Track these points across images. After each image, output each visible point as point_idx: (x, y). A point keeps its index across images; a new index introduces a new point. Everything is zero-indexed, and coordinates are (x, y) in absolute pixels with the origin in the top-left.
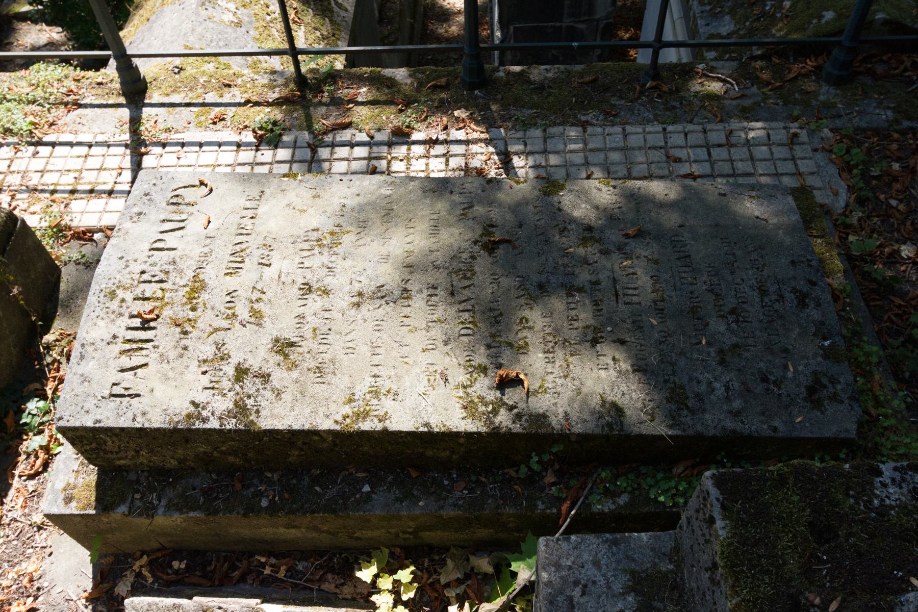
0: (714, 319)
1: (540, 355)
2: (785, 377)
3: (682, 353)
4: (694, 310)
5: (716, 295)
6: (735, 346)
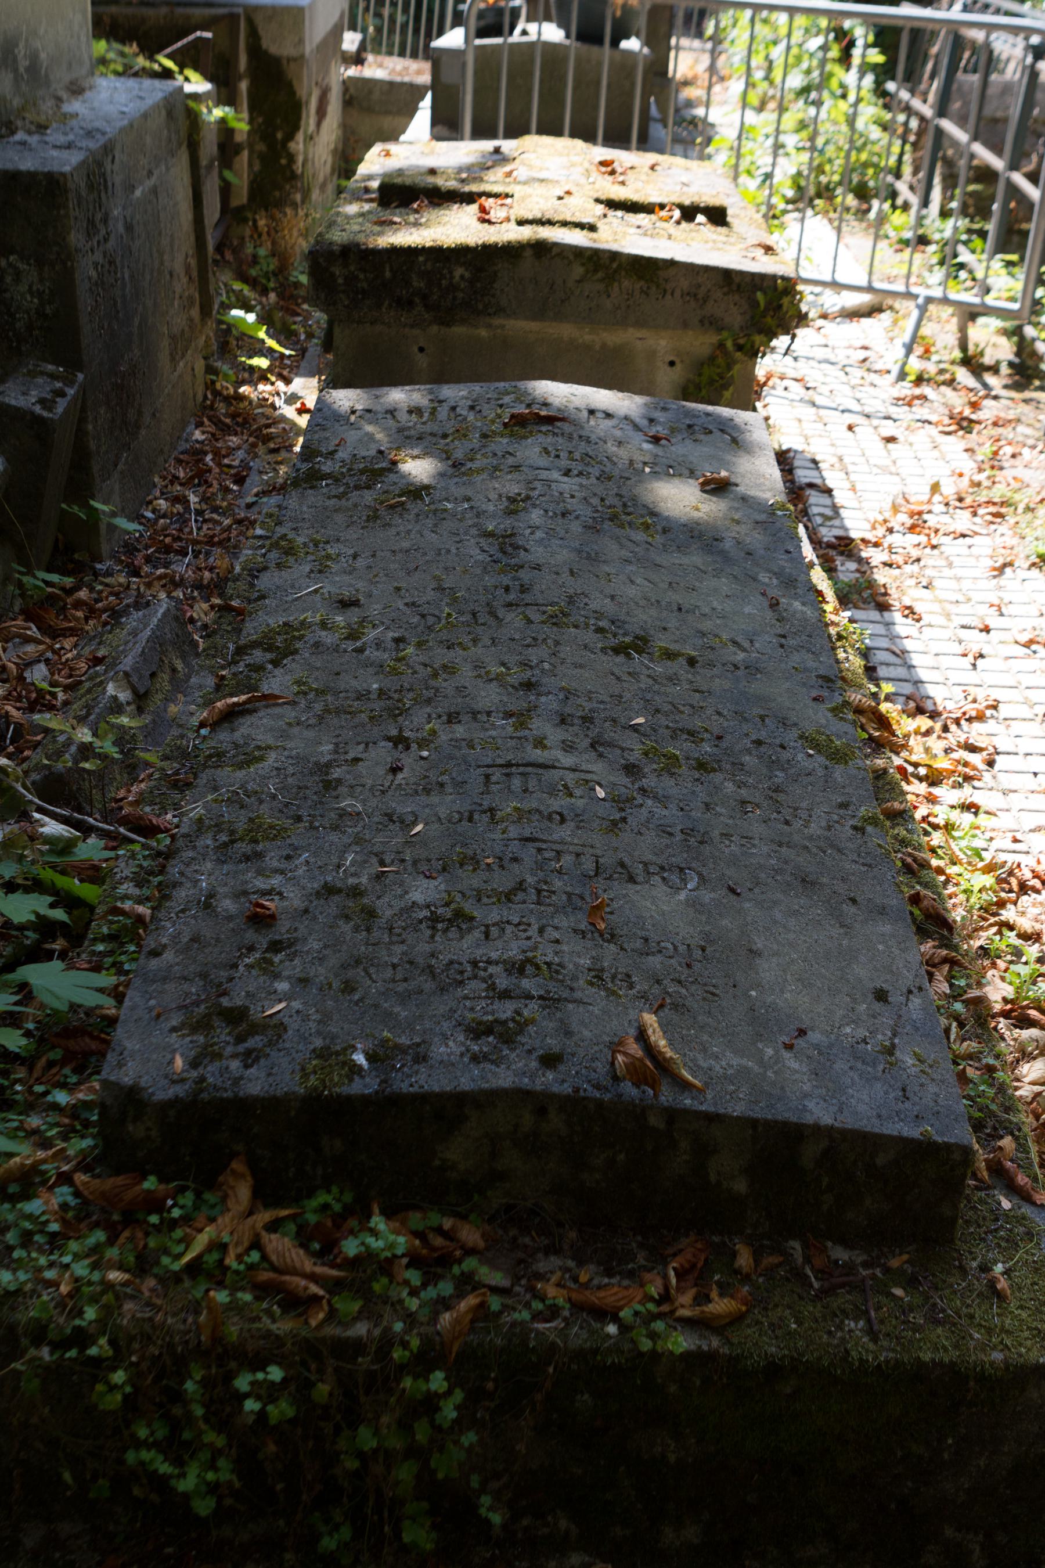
0: (443, 887)
1: (375, 686)
6: (371, 913)
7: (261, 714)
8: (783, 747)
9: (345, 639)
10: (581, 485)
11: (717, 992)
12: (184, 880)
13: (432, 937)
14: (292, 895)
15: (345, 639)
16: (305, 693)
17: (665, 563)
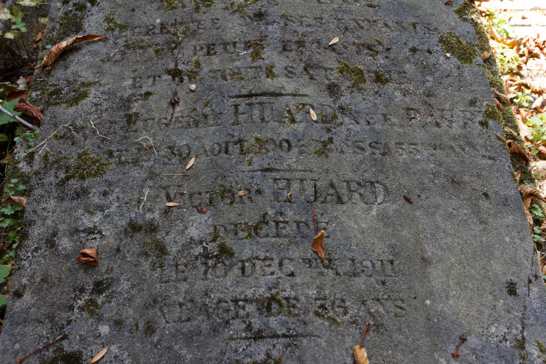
0: (210, 222)
1: (158, 21)
2: (100, 319)
3: (152, 175)
4: (227, 193)
5: (256, 228)
6: (162, 250)
7: (84, 51)
8: (429, 52)
11: (403, 305)
12: (35, 218)
13: (206, 273)
14: (108, 233)
16: (113, 30)
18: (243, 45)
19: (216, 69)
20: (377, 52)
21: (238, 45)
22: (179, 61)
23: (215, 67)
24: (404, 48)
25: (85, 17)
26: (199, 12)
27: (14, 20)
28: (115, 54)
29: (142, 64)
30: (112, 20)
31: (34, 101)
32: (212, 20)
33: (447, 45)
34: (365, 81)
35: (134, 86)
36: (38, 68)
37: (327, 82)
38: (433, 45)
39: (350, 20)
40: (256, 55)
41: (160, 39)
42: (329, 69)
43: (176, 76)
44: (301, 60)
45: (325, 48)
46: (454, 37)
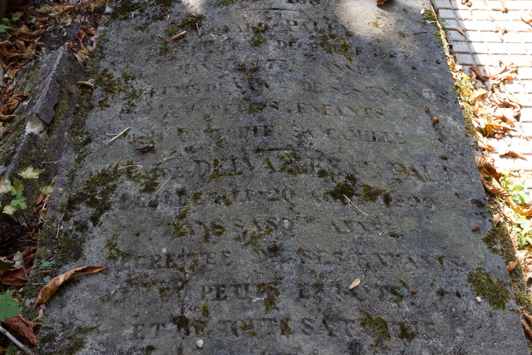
1: (164, 250)
7: (82, 285)
8: (458, 295)
9: (144, 191)
10: (301, 11)
15: (144, 191)
16: (115, 258)
17: (361, 88)
18: (255, 289)
19: (226, 319)
20: (402, 297)
21: (250, 288)
22: (185, 306)
23: (225, 317)
24: (430, 291)
25: (86, 240)
26: (208, 241)
27: (14, 193)
28: (116, 292)
29: (145, 307)
30: (114, 246)
31: (27, 312)
32: (223, 252)
33: (478, 286)
34: (390, 337)
35: (135, 336)
36: (34, 269)
37: (348, 339)
38: (462, 285)
39: (372, 254)
40: (270, 303)
41: (166, 275)
42: (350, 321)
43: (182, 326)
44: (319, 310)
45: (346, 293)
46: (484, 274)
